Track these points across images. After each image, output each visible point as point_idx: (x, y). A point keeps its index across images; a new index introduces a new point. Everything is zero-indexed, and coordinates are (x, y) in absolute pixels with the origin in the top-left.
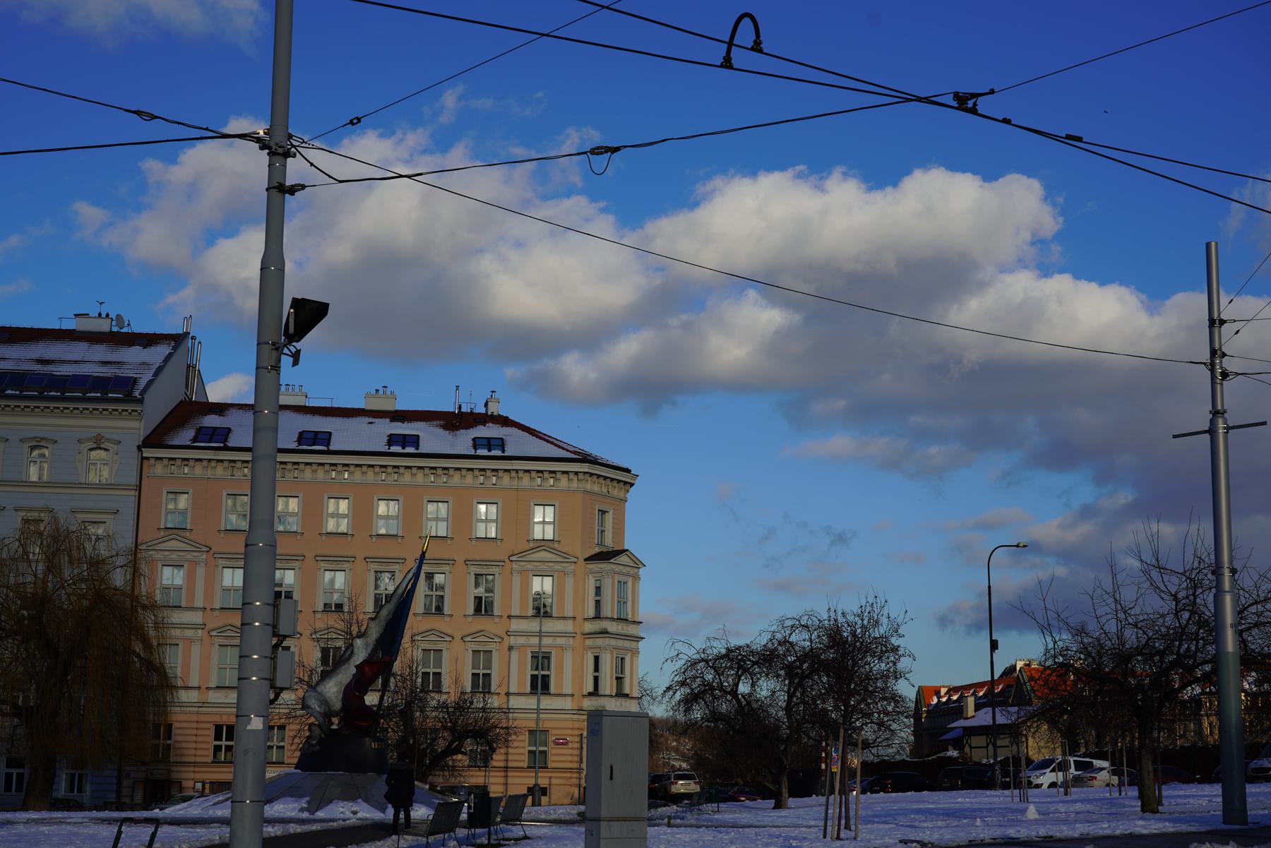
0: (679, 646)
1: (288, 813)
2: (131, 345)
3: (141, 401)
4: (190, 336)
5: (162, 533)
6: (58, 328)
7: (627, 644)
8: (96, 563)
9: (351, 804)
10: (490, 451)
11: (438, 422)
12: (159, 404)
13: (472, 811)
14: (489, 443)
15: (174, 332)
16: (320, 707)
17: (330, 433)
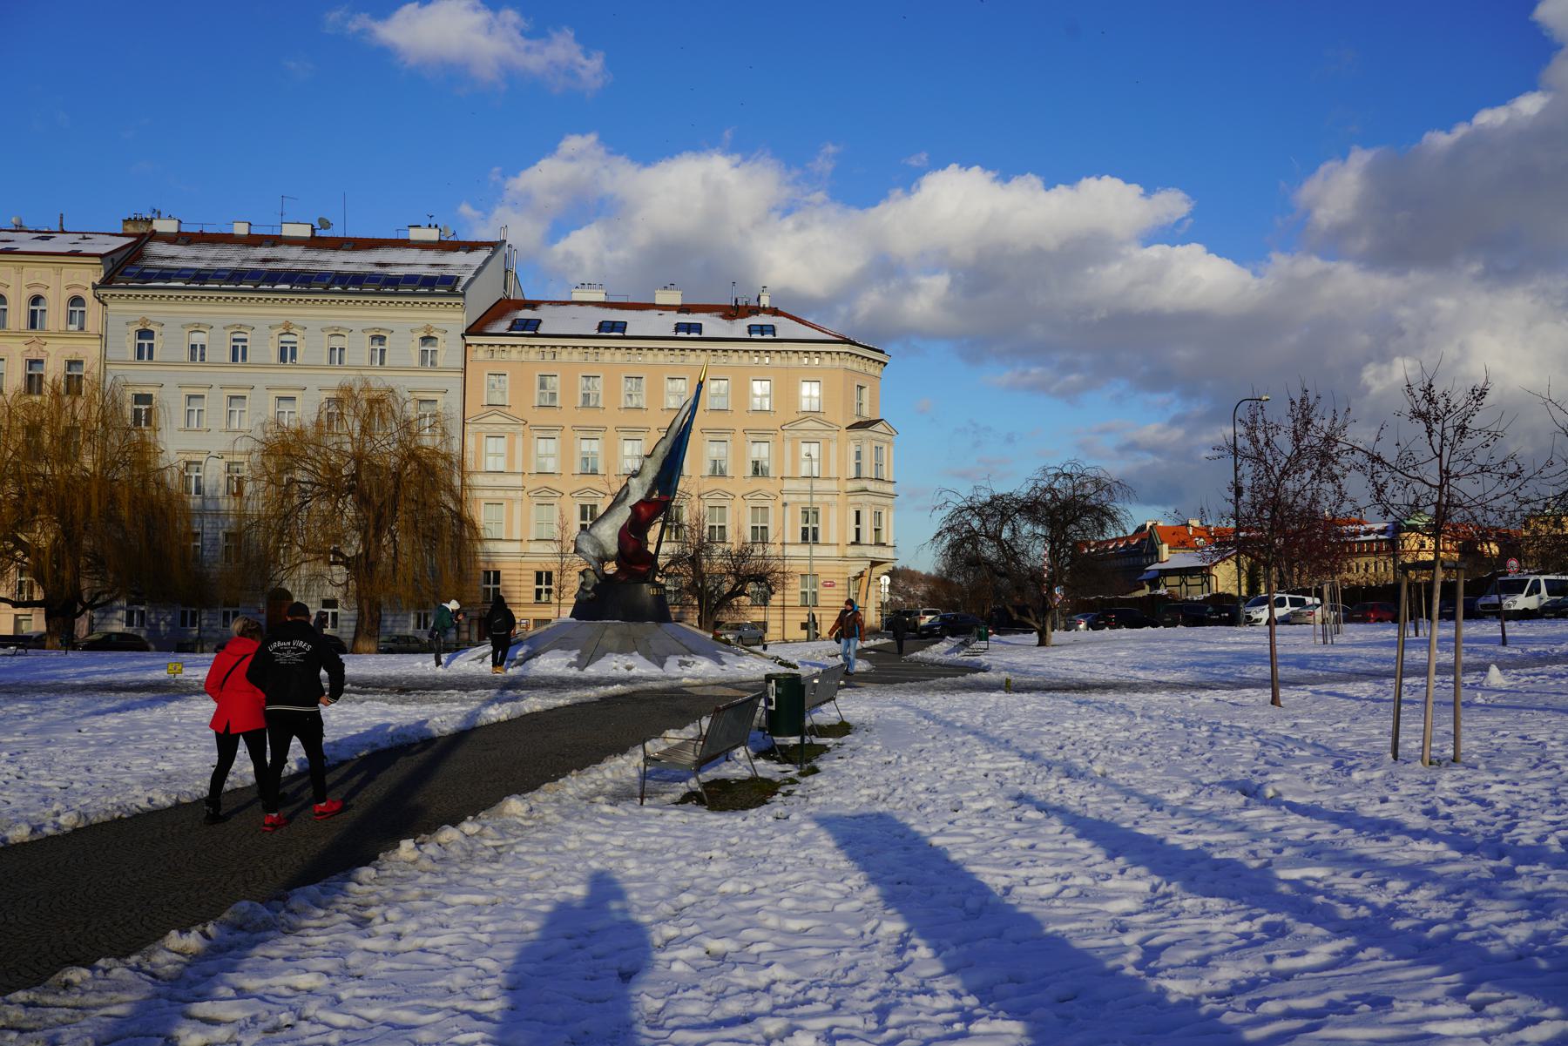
3: (463, 295)
4: (507, 244)
5: (485, 409)
8: (407, 424)
11: (718, 314)
12: (482, 297)
13: (773, 708)
14: (762, 329)
15: (493, 240)
16: (594, 551)
17: (626, 323)
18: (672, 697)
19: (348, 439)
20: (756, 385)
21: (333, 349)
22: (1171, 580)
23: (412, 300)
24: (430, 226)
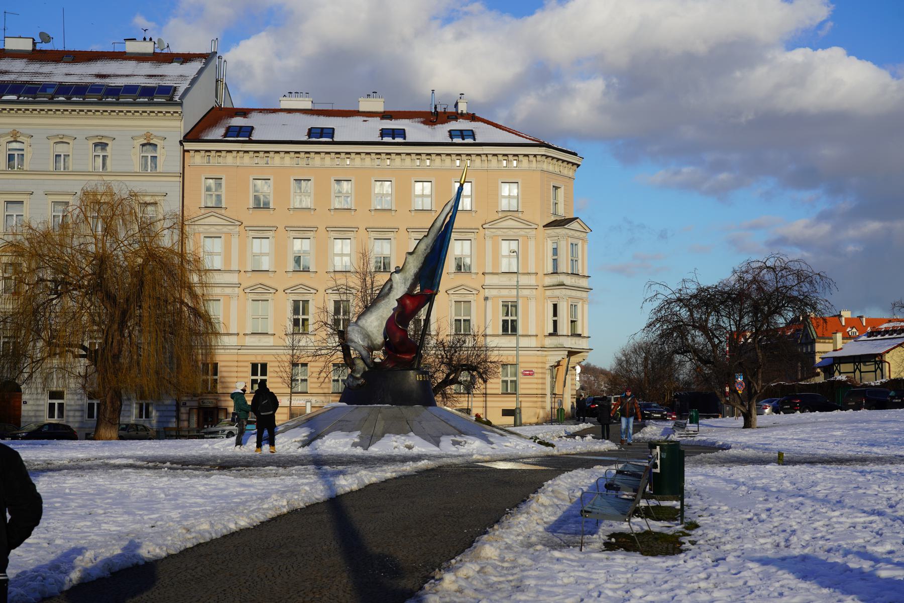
0: (655, 287)
1: (341, 448)
2: (171, 62)
4: (218, 55)
5: (203, 211)
6: (112, 50)
9: (403, 438)
10: (463, 139)
11: (419, 119)
14: (462, 134)
16: (363, 341)
17: (333, 129)
18: (478, 470)
19: (90, 239)
20: (418, 187)
21: (58, 156)
22: (845, 367)
23: (132, 109)
24: (145, 39)
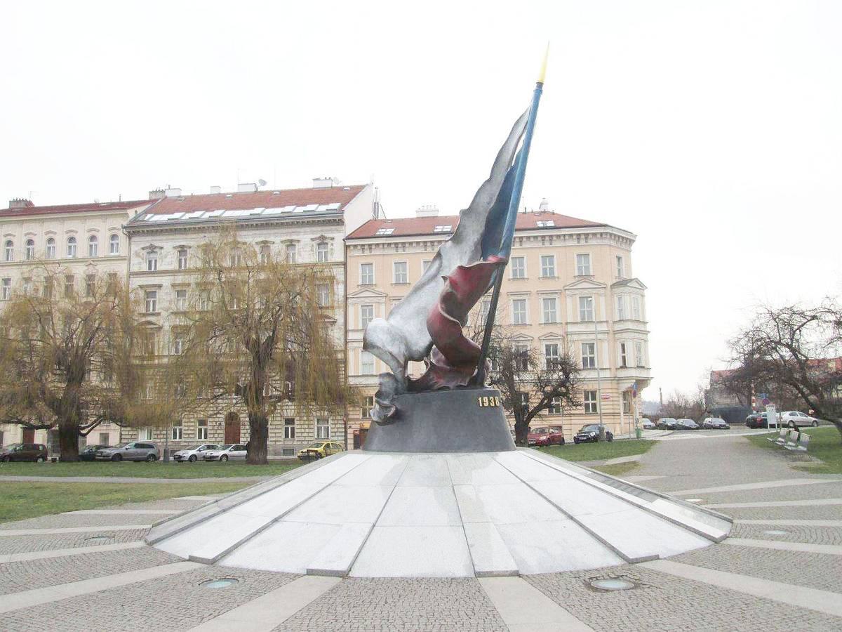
4: (374, 186)
7: (641, 336)
